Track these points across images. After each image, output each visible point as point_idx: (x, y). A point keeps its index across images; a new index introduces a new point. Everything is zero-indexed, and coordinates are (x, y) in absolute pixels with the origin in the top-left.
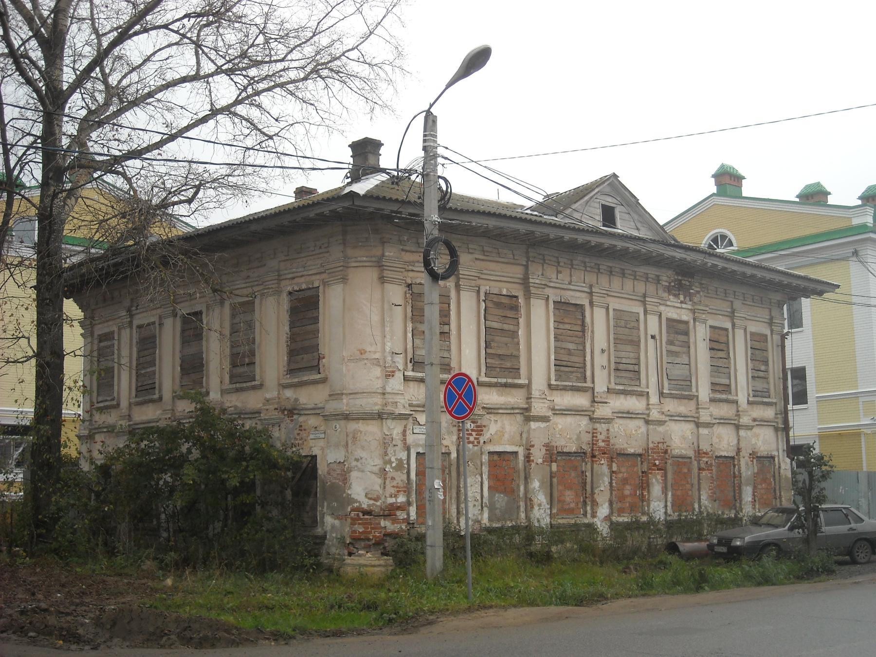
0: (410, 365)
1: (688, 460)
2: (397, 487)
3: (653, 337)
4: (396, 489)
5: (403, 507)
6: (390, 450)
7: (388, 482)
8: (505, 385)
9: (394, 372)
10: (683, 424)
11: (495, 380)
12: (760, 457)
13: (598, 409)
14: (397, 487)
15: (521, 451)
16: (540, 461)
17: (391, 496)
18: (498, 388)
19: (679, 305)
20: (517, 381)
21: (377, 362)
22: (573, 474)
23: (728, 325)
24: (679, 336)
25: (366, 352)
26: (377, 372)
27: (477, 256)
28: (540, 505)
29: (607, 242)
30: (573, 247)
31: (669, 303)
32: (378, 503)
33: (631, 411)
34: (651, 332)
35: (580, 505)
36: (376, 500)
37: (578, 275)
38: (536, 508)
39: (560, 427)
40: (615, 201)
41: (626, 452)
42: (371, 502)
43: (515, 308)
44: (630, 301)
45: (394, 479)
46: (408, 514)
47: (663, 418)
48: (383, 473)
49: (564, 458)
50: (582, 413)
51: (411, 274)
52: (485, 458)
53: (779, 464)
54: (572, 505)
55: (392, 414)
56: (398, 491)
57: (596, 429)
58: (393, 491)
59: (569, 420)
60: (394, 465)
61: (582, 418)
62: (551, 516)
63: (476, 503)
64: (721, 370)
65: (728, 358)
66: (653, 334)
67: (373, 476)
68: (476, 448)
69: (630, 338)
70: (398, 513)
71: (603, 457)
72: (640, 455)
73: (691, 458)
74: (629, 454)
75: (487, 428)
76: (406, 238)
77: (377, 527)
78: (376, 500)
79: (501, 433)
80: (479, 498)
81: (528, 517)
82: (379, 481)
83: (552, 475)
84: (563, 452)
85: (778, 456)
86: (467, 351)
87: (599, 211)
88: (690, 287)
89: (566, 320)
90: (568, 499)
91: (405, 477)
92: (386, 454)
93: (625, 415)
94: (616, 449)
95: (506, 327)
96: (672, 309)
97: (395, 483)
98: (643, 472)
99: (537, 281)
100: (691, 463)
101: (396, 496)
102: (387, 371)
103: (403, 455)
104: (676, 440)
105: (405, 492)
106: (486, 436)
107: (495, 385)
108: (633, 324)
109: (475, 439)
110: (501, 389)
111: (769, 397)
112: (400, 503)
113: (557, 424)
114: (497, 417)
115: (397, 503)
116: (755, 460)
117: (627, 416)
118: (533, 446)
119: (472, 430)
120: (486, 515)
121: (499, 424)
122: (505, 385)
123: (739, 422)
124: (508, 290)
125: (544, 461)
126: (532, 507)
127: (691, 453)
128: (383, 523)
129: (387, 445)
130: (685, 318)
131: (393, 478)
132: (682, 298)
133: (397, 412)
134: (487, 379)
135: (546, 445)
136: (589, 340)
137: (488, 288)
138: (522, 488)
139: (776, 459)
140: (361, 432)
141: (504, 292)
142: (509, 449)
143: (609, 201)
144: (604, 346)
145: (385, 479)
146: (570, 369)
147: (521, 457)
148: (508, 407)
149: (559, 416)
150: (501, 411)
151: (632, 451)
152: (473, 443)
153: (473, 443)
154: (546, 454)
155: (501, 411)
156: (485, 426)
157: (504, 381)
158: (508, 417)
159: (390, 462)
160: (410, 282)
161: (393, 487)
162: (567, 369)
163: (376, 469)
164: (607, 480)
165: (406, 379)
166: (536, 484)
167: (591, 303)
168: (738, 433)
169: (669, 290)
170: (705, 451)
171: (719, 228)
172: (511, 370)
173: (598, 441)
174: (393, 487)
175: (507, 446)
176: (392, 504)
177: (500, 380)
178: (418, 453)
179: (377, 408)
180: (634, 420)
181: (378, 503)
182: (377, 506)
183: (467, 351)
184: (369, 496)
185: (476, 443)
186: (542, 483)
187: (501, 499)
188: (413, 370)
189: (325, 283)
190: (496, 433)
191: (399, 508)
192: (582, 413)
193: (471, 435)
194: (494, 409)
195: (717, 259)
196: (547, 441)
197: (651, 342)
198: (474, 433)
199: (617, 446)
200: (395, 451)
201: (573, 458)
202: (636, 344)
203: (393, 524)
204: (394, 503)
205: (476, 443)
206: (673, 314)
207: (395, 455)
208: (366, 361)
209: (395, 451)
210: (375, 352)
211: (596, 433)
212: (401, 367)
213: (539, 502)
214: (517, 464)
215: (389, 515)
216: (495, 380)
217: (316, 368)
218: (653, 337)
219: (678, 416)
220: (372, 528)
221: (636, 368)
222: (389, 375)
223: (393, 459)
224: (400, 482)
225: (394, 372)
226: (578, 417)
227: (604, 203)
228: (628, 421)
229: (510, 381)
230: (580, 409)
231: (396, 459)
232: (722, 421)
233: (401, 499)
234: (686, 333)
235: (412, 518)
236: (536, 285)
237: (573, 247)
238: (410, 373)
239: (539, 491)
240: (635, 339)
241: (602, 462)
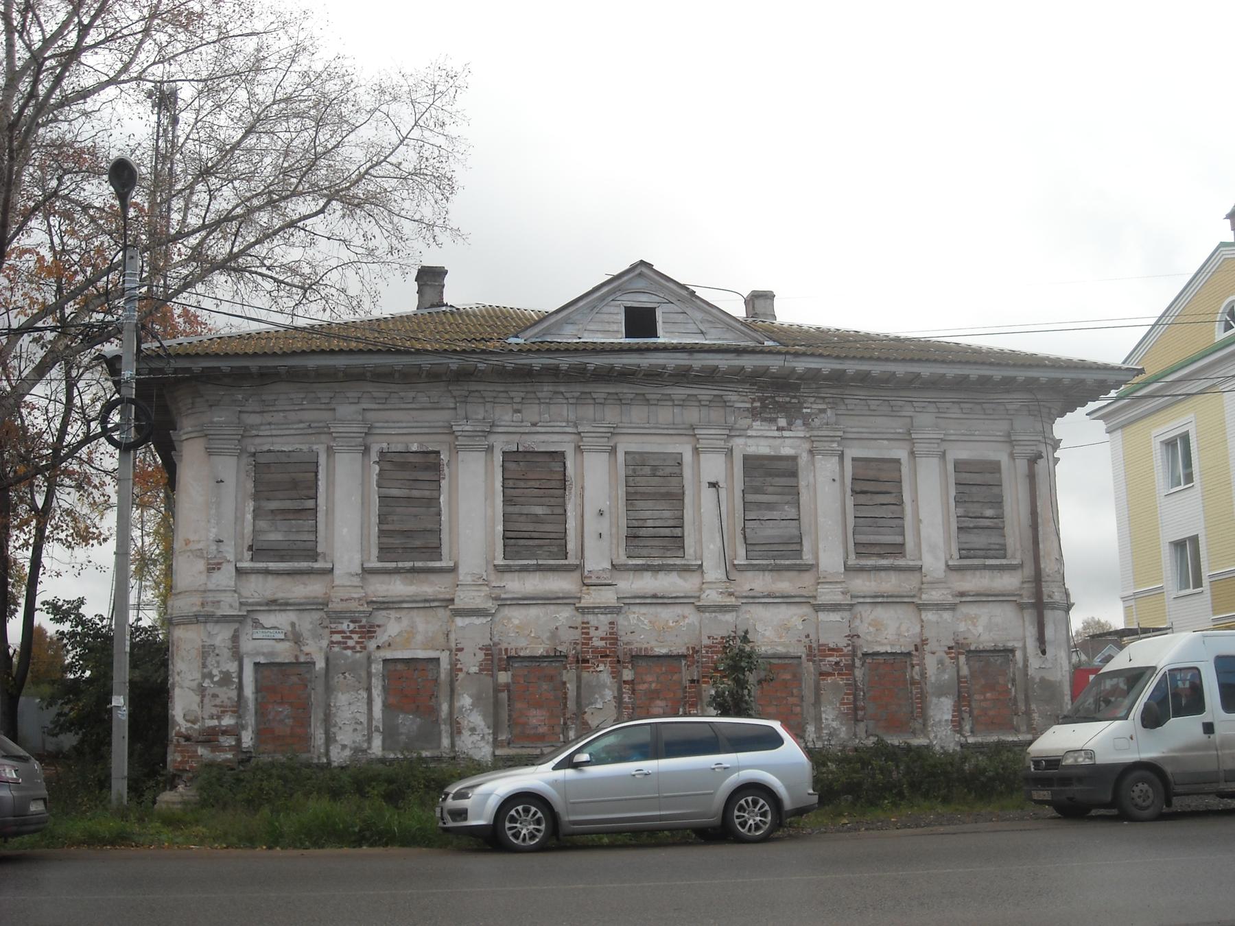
0: (247, 555)
1: (795, 661)
2: (221, 706)
3: (713, 485)
4: (220, 710)
5: (235, 732)
6: (211, 660)
7: (206, 700)
8: (413, 570)
9: (220, 564)
10: (783, 608)
11: (393, 565)
12: (977, 652)
13: (588, 594)
14: (221, 706)
15: (444, 658)
16: (474, 669)
17: (212, 718)
18: (403, 575)
19: (776, 434)
20: (437, 564)
21: (199, 554)
22: (545, 686)
23: (901, 453)
24: (777, 479)
25: (190, 542)
26: (201, 565)
27: (365, 406)
28: (473, 730)
29: (646, 361)
30: (580, 375)
31: (750, 433)
32: (196, 727)
33: (667, 595)
34: (707, 477)
35: (558, 729)
36: (194, 722)
37: (566, 411)
38: (466, 733)
39: (516, 622)
40: (657, 299)
41: (650, 653)
42: (189, 725)
43: (436, 467)
44: (668, 437)
45: (217, 696)
46: (239, 741)
47: (731, 601)
48: (201, 691)
49: (526, 664)
50: (559, 601)
51: (257, 440)
52: (377, 668)
53: (1026, 660)
54: (541, 730)
55: (212, 616)
56: (223, 712)
57: (588, 623)
58: (214, 711)
59: (533, 612)
60: (216, 679)
61: (561, 608)
62: (496, 744)
63: (359, 727)
64: (881, 522)
65: (900, 503)
66: (713, 480)
67: (192, 693)
68: (358, 655)
69: (663, 490)
70: (222, 739)
71: (603, 662)
72: (685, 656)
73: (800, 657)
74: (659, 657)
75: (382, 629)
76: (240, 397)
77: (194, 755)
78: (194, 722)
79: (411, 633)
80: (364, 719)
81: (453, 745)
82: (198, 699)
83: (497, 689)
84: (519, 657)
85: (1024, 648)
86: (345, 530)
87: (622, 317)
88: (800, 406)
89: (530, 476)
90: (534, 721)
91: (233, 694)
92: (204, 666)
93: (648, 601)
94: (631, 650)
95: (416, 493)
96: (763, 442)
97: (218, 702)
98: (692, 681)
99: (467, 428)
100: (800, 664)
101: (219, 718)
102: (209, 564)
103: (232, 667)
104: (767, 633)
105: (234, 712)
106: (382, 638)
107: (397, 571)
108: (668, 470)
109: (357, 643)
110: (409, 575)
111: (1005, 557)
112: (227, 726)
113: (509, 619)
114: (403, 613)
115: (220, 725)
116: (962, 659)
117: (654, 601)
118: (461, 650)
119: (352, 632)
120: (377, 742)
121: (405, 623)
122: (413, 570)
123: (920, 598)
124: (421, 444)
125: (481, 670)
126: (459, 732)
127: (800, 651)
128: (201, 751)
129: (206, 655)
130: (787, 451)
131: (215, 696)
132: (782, 422)
133: (219, 613)
134: (380, 565)
135: (487, 650)
136: (620, 496)
137: (385, 445)
138: (445, 707)
139: (1019, 654)
140: (181, 639)
141: (414, 448)
142: (421, 654)
143: (642, 301)
144: (605, 504)
145: (203, 696)
146: (537, 542)
147: (445, 665)
148: (418, 599)
149: (513, 608)
150: (405, 605)
151: (664, 651)
152: (353, 648)
153: (353, 648)
154: (485, 660)
155: (405, 605)
156: (379, 626)
157: (408, 564)
158: (422, 612)
159: (211, 676)
160: (253, 450)
161: (215, 706)
162: (531, 542)
163: (194, 684)
164: (609, 694)
165: (239, 572)
166: (466, 701)
167: (579, 449)
168: (921, 615)
169: (754, 414)
170: (831, 646)
171: (1228, 296)
172: (424, 550)
173: (591, 639)
174: (215, 706)
175: (419, 651)
176: (214, 728)
177: (400, 565)
178: (257, 664)
179: (195, 609)
180: (669, 606)
181: (196, 727)
182: (195, 730)
183: (345, 530)
184: (187, 718)
185: (358, 648)
186: (477, 701)
187: (408, 723)
188: (252, 560)
189: (455, 450)
190: (400, 634)
191: (226, 732)
192: (559, 601)
193: (350, 638)
194: (393, 602)
195: (811, 359)
196: (488, 642)
197: (708, 495)
198: (355, 637)
199: (634, 646)
200: (218, 662)
201: (545, 664)
202: (677, 498)
203: (213, 751)
204: (216, 726)
205: (358, 648)
206: (761, 448)
207: (218, 667)
208: (188, 554)
209: (218, 662)
210: (199, 541)
211: (588, 628)
212: (231, 557)
213: (471, 725)
214: (438, 672)
215: (209, 741)
216: (393, 565)
217: (435, 551)
218: (713, 485)
219: (768, 596)
220: (190, 757)
221: (677, 532)
222: (214, 569)
223: (215, 672)
224: (226, 700)
225: (220, 564)
226: (552, 607)
227: (629, 304)
228: (659, 609)
229: (419, 564)
230: (550, 595)
231: (221, 672)
232: (880, 600)
233: (228, 721)
234: (794, 474)
235: (244, 745)
236: (467, 434)
237: (580, 375)
238: (246, 564)
239: (471, 710)
240: (677, 490)
241: (601, 668)
